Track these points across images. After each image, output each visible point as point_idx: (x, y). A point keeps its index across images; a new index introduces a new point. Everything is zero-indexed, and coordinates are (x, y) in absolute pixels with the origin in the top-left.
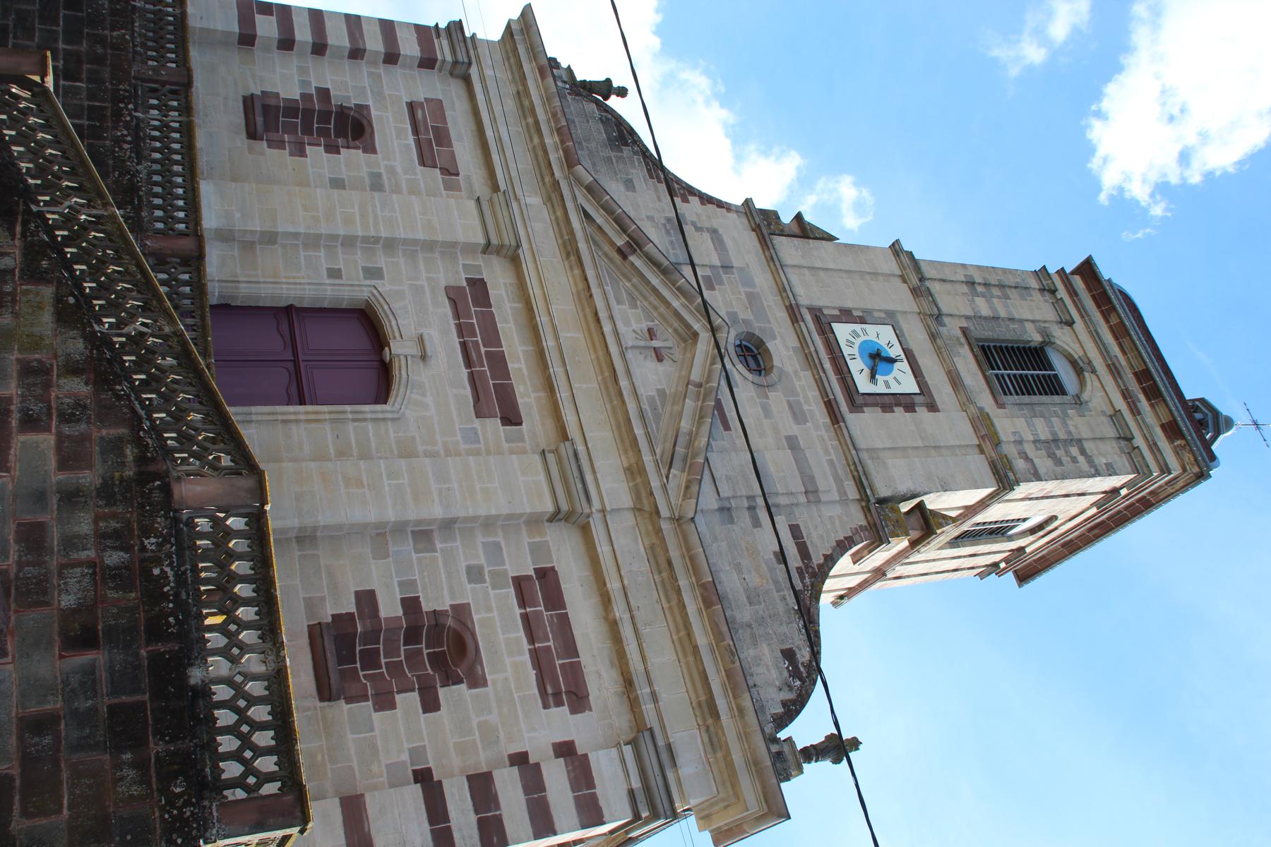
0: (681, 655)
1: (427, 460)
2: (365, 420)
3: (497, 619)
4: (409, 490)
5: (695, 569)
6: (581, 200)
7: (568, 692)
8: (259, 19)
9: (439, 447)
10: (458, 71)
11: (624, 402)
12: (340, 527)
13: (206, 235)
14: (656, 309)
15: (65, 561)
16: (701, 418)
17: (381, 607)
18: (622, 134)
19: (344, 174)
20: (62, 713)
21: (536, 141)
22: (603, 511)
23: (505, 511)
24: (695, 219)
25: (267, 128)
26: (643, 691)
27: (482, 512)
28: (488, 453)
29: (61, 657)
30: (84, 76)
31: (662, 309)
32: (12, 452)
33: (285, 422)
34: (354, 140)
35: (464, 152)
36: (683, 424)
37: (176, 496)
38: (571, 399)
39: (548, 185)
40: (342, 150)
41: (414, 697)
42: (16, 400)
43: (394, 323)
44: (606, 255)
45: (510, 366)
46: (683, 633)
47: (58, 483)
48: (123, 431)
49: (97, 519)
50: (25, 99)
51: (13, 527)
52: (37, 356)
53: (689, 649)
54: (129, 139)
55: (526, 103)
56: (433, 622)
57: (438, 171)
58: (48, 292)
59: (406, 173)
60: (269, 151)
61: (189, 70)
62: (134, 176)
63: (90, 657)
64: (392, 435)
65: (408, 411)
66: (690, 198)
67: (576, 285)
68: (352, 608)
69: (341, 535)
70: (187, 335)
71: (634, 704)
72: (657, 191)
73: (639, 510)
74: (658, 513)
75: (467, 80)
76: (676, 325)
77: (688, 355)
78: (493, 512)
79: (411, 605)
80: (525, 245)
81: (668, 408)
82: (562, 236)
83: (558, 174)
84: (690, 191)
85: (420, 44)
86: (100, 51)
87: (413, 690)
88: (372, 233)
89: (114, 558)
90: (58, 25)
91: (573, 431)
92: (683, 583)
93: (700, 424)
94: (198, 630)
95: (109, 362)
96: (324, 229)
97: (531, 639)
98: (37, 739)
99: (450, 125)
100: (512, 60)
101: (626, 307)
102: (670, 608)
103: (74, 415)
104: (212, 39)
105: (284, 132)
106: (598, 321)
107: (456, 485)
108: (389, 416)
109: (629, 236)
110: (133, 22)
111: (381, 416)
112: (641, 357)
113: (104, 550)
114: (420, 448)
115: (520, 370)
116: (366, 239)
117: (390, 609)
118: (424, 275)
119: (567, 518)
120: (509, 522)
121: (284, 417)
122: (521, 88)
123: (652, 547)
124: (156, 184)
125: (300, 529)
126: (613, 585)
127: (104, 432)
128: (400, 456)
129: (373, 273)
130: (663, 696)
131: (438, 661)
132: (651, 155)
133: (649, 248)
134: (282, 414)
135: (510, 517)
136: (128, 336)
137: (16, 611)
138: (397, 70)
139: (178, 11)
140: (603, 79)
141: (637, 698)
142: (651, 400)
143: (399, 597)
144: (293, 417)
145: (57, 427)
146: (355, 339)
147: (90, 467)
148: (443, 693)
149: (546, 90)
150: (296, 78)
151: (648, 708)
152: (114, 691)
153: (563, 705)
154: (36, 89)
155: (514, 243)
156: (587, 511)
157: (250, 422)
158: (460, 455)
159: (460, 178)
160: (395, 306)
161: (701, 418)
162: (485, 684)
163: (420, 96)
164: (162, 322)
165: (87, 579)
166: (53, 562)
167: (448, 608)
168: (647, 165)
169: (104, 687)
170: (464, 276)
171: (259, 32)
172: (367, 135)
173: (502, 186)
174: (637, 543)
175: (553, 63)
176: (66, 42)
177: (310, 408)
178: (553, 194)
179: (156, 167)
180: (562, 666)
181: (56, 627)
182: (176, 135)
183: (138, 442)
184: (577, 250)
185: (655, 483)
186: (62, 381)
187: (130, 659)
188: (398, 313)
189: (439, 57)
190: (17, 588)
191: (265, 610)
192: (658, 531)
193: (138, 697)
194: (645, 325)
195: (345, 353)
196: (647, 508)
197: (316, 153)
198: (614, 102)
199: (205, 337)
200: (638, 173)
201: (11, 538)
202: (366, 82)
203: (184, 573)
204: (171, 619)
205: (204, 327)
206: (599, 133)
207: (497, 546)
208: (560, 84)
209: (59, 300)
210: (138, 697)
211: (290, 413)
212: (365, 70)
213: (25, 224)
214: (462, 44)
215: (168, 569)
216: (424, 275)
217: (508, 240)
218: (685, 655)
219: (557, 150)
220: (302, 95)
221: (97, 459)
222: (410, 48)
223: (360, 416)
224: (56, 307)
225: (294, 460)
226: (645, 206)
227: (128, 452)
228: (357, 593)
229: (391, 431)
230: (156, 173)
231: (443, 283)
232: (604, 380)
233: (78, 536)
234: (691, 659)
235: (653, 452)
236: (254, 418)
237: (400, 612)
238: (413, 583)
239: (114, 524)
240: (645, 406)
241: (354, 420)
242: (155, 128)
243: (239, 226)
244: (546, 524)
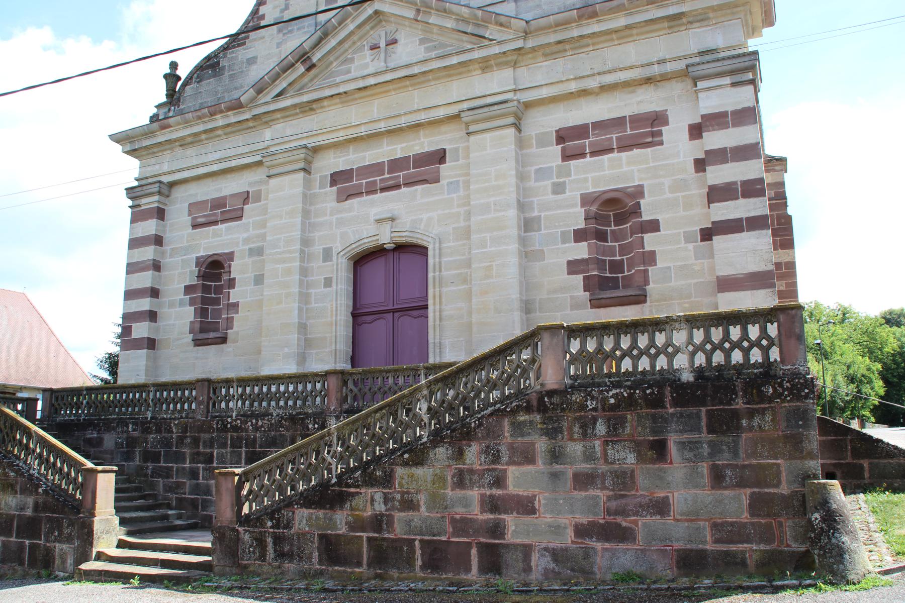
0: (631, 39)
1: (473, 219)
2: (440, 263)
3: (593, 175)
4: (495, 233)
5: (566, 23)
6: (268, 98)
7: (652, 126)
8: (135, 335)
9: (462, 210)
10: (165, 190)
11: (431, 71)
12: (521, 283)
13: (300, 372)
14: (354, 43)
15: (602, 461)
16: (445, 11)
17: (580, 257)
18: (210, 66)
19: (251, 275)
20: (711, 463)
21: (220, 132)
22: (515, 91)
23: (513, 164)
24: (278, 10)
25: (216, 330)
26: (656, 70)
27: (513, 181)
28: (468, 174)
29: (671, 463)
30: (209, 451)
31: (355, 38)
32: (521, 493)
33: (441, 319)
34: (223, 268)
35: (229, 187)
36: (449, 26)
37: (555, 387)
38: (427, 111)
39: (255, 124)
40: (232, 277)
41: (648, 238)
42: (483, 491)
43: (365, 241)
44: (312, 80)
45: (399, 156)
46: (614, 36)
47: (544, 464)
48: (506, 422)
49: (572, 439)
50: (251, 486)
51: (576, 492)
52: (449, 478)
53: (628, 32)
54: (254, 421)
55: (189, 140)
56: (594, 220)
57: (245, 207)
58: (400, 471)
59: (248, 230)
60: (235, 329)
61: (198, 381)
62: (282, 418)
63: (672, 445)
64: (451, 244)
65: (434, 232)
66: (261, 13)
67: (336, 104)
68: (580, 277)
69: (527, 283)
70: (431, 377)
71: (665, 78)
72: (255, 40)
73: (515, 63)
74: (519, 49)
75: (172, 185)
76: (368, 28)
77: (392, 19)
78: (514, 172)
79: (580, 236)
80: (304, 142)
81: (435, 37)
82: (297, 114)
83: (247, 116)
84: (255, 13)
85: (146, 219)
86: (189, 440)
87: (642, 238)
88: (297, 255)
89: (601, 428)
90: (172, 467)
91: (453, 110)
92: (575, 33)
93: (451, 12)
94: (654, 374)
95: (453, 431)
96: (296, 290)
97: (610, 150)
98: (727, 478)
99: (209, 197)
100: (155, 150)
101: (353, 67)
102: (593, 44)
103: (493, 454)
104: (153, 366)
105: (220, 318)
106: (365, 88)
107: (492, 199)
108: (437, 245)
109: (297, 62)
110: (164, 419)
111: (437, 251)
112: (393, 55)
113: (595, 435)
114: (462, 224)
115: (402, 149)
116: (302, 260)
117: (582, 251)
118: (328, 218)
119: (519, 119)
120: (521, 162)
121: (438, 320)
122: (177, 144)
123: (545, 55)
124: (286, 403)
125: (521, 311)
126: (573, 87)
127: (507, 434)
128: (469, 238)
129: (327, 254)
130: (661, 55)
131: (620, 219)
132: (226, 43)
133: (307, 46)
134: (435, 321)
135: (517, 161)
136: (430, 419)
137: (637, 490)
138: (167, 237)
139: (152, 389)
140: (164, 81)
141: (661, 75)
142: (428, 50)
143: (573, 244)
144: (437, 314)
145: (503, 465)
146: (376, 270)
147: (533, 444)
148: (646, 217)
149: (179, 124)
150: (178, 309)
151: (670, 67)
152: (698, 430)
153: (661, 130)
154: (243, 479)
155: (304, 150)
156: (515, 103)
157: (440, 343)
158: (469, 195)
159: (250, 190)
160: (353, 240)
161: (445, 11)
162: (642, 186)
163: (187, 220)
164: (419, 396)
165: (616, 446)
166: (603, 467)
167: (583, 210)
168: (234, 47)
169: (694, 436)
170: (329, 189)
171: (145, 335)
172: (220, 258)
173: (258, 158)
174: (541, 67)
175: (154, 119)
176: (184, 461)
177: (430, 302)
178: (263, 120)
179: (273, 403)
180: (631, 129)
181: (651, 466)
182: (248, 389)
183: (515, 412)
184: (308, 102)
185: (497, 50)
186: (468, 462)
187: (675, 419)
188: (357, 237)
189: (156, 205)
190: (621, 490)
191: (642, 328)
192: (534, 49)
193: (703, 415)
194: (367, 52)
195: (388, 280)
196: (515, 57)
197: (235, 295)
198: (183, 72)
199: (403, 370)
200: (241, 54)
201: (584, 494)
202: (178, 259)
203: (612, 382)
204: (648, 392)
205: (395, 371)
206: (209, 84)
207: (538, 171)
208: (171, 114)
209: (406, 464)
210: (703, 415)
211: (435, 316)
212: (168, 260)
213: (348, 486)
214: (145, 188)
215: (611, 393)
216: (328, 218)
217: (301, 154)
218: (631, 35)
219: (227, 116)
220: (191, 305)
221: (527, 439)
222: (150, 227)
223: (437, 267)
224: (412, 466)
225: (470, 313)
226: (268, 51)
227: (522, 419)
228: (569, 273)
229: (449, 244)
230: (278, 404)
231: (334, 204)
232: (412, 85)
233: (584, 452)
234: (635, 31)
235: (472, 50)
236: (437, 341)
237: (585, 244)
238: (563, 233)
239: (576, 428)
240: (433, 54)
241: (440, 271)
242: (244, 403)
243: (295, 349)
244: (523, 134)
